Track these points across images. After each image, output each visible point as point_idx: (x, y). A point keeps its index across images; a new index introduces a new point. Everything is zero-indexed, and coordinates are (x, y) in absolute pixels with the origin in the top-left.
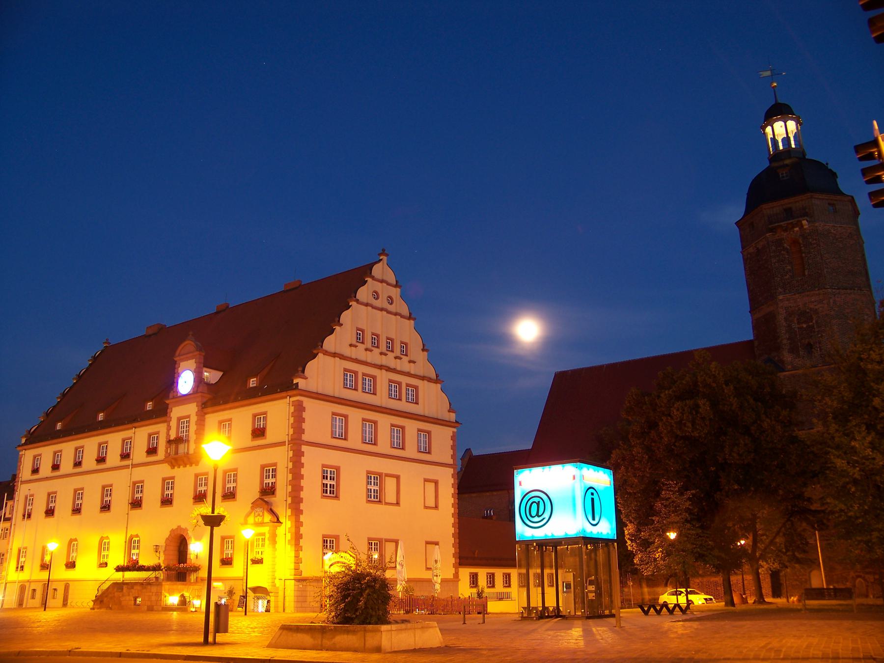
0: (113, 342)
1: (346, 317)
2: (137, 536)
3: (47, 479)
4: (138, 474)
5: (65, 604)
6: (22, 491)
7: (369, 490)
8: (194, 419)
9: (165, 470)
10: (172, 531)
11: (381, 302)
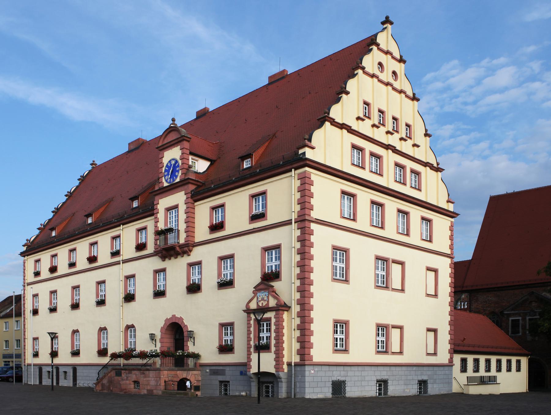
0: (98, 163)
8: (182, 208)
9: (156, 263)
10: (167, 320)
11: (386, 76)
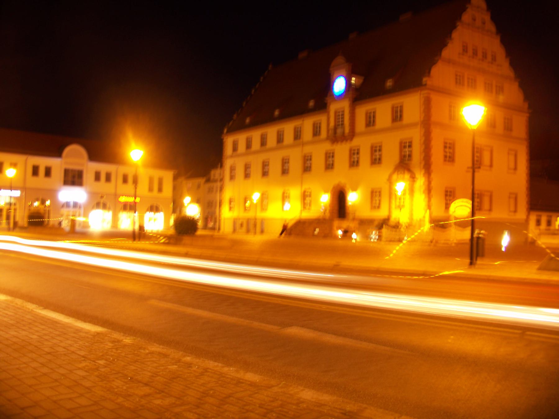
1: (455, 35)
2: (309, 188)
4: (308, 149)
5: (262, 232)
6: (228, 163)
9: (327, 146)
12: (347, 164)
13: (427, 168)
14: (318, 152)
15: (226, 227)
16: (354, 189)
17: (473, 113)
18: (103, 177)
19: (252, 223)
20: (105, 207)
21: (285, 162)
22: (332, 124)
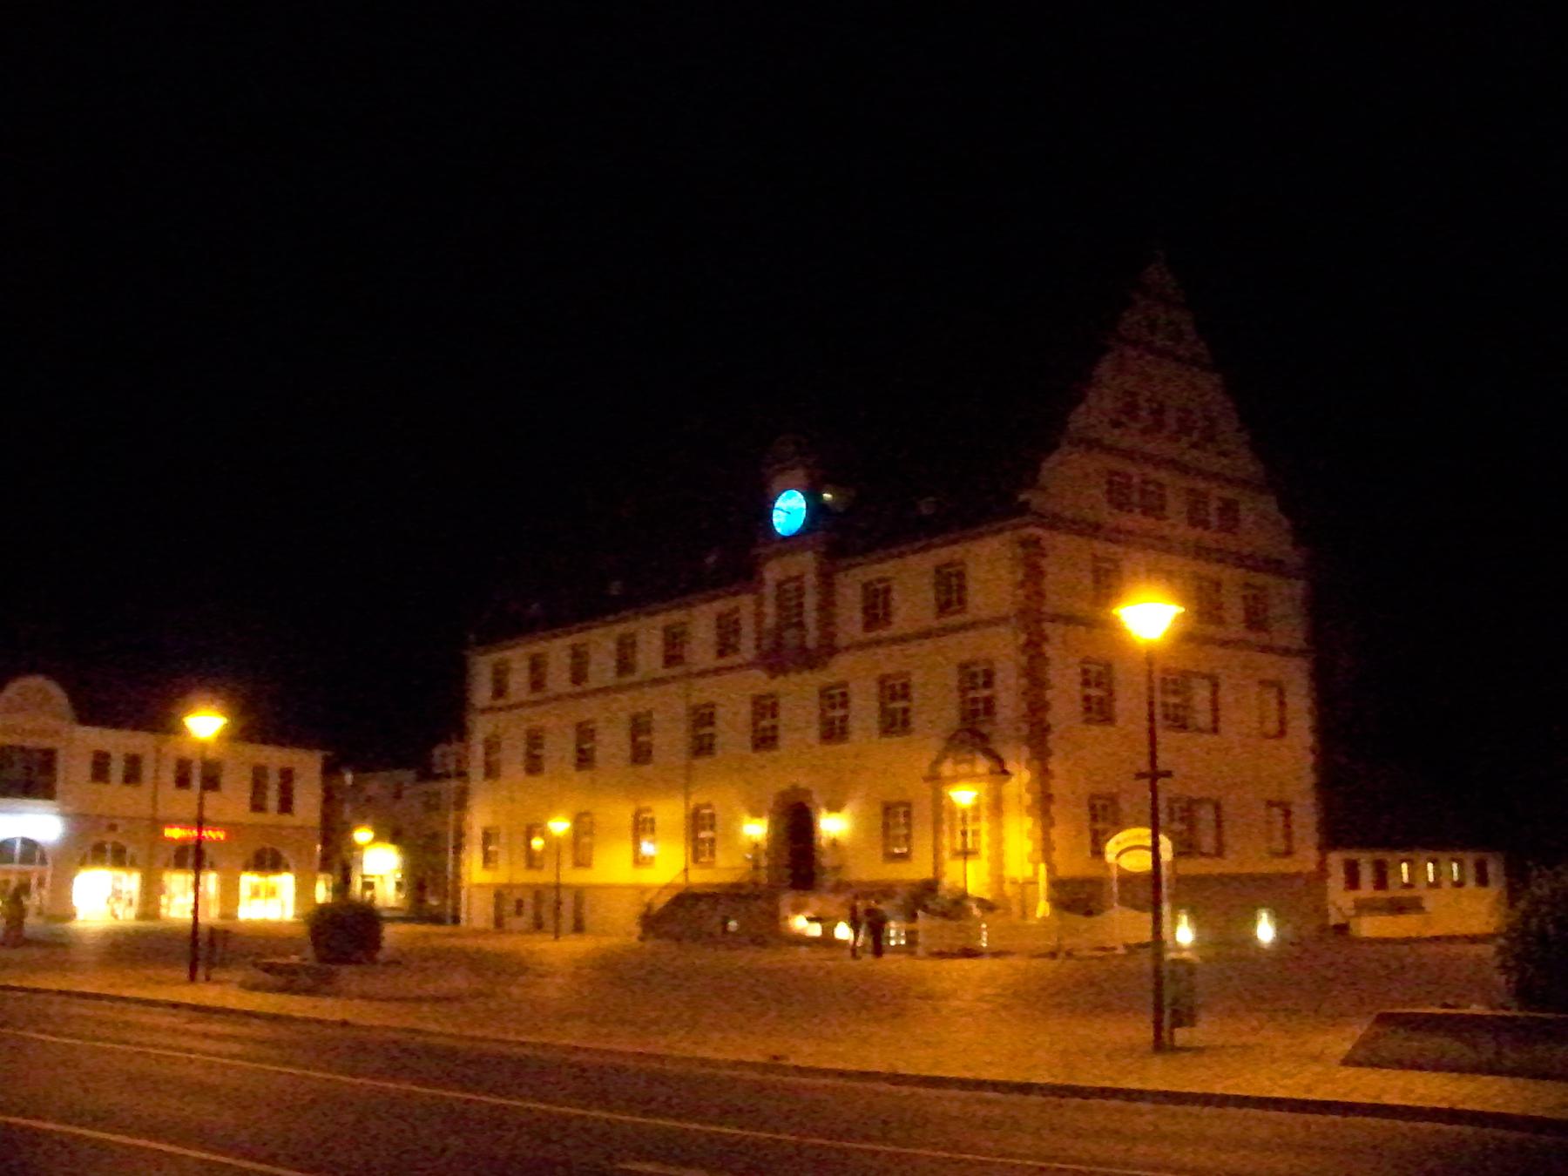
2: (709, 806)
3: (605, 690)
4: (704, 692)
5: (579, 927)
6: (481, 728)
7: (1087, 699)
8: (811, 579)
9: (759, 681)
12: (813, 733)
13: (1038, 739)
14: (733, 698)
15: (476, 910)
16: (835, 807)
17: (1149, 616)
18: (117, 769)
19: (551, 896)
20: (119, 858)
21: (639, 726)
22: (770, 622)
